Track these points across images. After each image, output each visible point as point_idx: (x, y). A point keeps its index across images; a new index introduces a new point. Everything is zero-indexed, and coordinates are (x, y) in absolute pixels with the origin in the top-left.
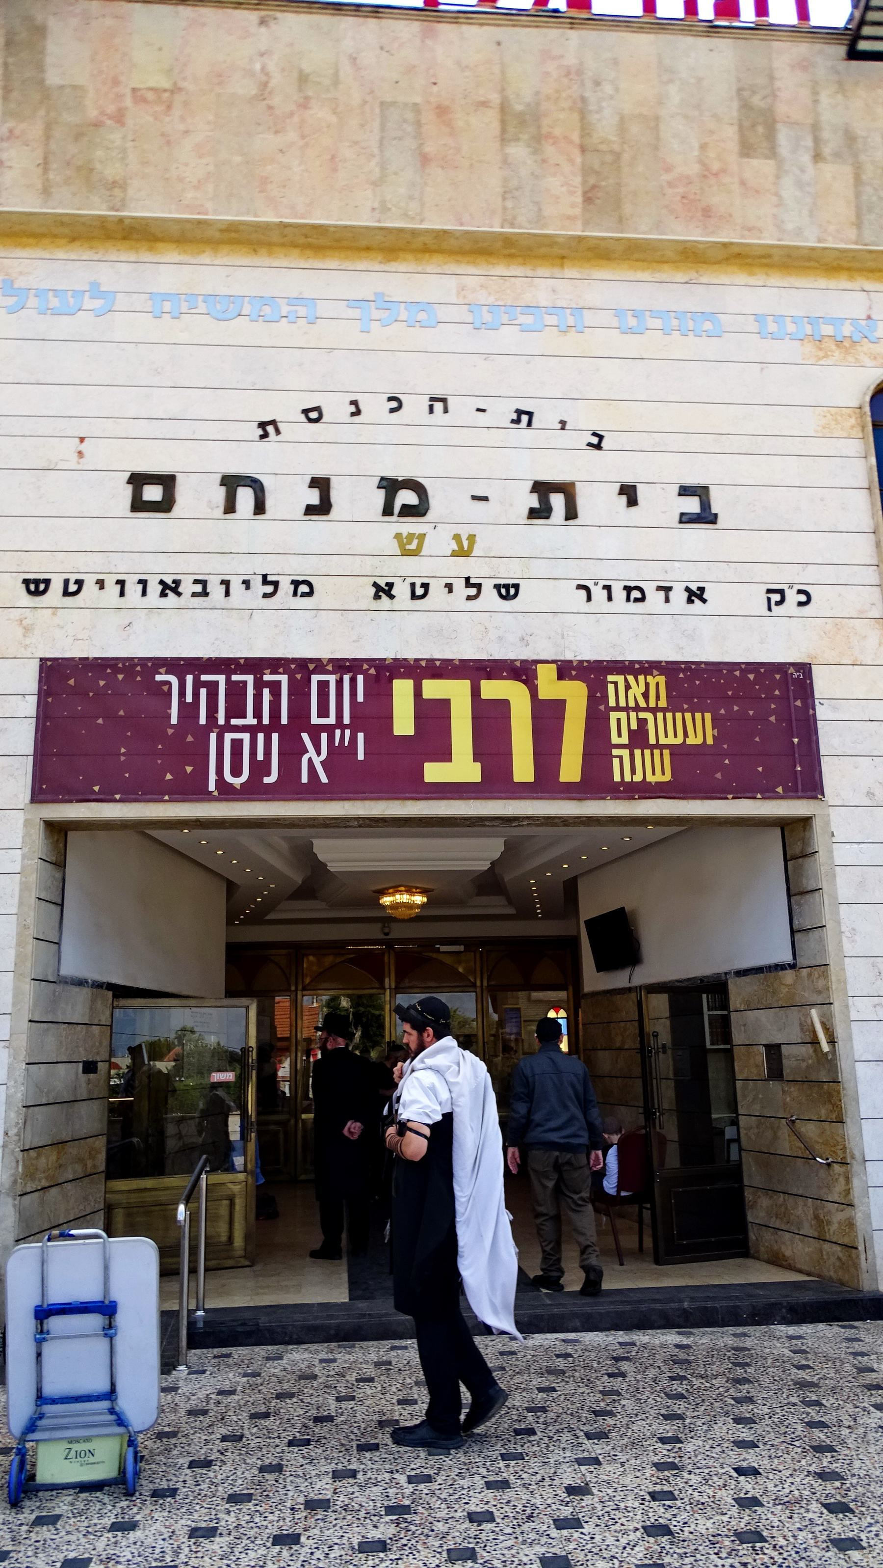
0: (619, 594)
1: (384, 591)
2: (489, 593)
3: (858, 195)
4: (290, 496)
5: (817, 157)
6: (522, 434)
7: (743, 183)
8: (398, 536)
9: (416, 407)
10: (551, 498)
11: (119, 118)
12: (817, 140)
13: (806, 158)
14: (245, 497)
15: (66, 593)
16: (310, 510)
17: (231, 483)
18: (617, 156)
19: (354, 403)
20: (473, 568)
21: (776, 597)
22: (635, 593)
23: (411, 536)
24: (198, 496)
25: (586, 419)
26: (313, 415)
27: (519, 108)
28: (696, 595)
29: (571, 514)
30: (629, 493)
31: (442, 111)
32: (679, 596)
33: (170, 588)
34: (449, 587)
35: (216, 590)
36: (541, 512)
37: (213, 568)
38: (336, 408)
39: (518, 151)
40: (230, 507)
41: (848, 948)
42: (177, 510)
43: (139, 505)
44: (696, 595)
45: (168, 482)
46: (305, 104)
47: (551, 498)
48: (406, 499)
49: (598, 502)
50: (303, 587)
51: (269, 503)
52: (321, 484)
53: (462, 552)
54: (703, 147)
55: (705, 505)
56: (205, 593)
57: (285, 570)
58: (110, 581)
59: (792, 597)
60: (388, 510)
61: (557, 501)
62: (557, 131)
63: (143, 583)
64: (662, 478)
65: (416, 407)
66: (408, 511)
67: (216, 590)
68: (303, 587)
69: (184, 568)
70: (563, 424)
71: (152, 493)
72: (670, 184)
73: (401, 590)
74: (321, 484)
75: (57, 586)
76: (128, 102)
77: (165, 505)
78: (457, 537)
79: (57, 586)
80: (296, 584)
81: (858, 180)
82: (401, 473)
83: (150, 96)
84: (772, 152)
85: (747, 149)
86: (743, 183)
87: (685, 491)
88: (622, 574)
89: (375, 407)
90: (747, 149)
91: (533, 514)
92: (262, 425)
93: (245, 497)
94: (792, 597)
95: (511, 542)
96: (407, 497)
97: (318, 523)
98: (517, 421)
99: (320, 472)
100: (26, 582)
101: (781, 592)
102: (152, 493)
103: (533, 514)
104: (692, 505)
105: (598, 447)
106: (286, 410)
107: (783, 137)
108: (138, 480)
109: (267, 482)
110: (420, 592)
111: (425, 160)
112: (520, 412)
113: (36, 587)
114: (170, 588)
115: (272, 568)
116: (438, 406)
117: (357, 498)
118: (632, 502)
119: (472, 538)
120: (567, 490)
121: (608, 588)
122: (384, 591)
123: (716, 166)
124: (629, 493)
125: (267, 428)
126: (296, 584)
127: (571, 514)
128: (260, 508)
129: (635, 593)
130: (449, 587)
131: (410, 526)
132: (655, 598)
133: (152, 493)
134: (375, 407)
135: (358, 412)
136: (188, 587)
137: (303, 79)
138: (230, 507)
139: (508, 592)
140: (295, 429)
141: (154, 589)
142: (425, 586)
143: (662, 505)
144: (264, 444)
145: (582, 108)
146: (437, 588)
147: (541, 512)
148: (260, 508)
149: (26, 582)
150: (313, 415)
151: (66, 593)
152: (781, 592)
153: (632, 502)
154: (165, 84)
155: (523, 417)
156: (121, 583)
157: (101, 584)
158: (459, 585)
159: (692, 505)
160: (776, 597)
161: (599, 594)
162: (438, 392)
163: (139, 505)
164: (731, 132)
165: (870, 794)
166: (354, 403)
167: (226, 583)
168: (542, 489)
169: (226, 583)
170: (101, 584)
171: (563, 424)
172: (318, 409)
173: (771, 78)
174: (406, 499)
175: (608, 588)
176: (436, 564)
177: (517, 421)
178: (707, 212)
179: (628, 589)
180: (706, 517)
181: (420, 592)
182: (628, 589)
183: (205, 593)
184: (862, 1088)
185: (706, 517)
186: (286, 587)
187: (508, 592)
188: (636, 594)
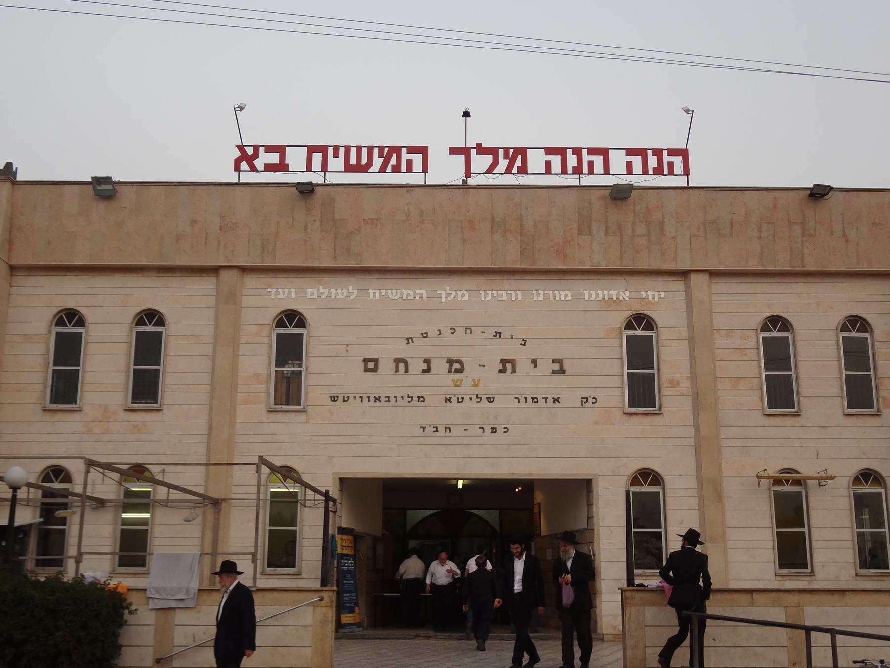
0: (529, 400)
1: (449, 400)
2: (484, 400)
3: (621, 247)
4: (417, 366)
5: (607, 233)
6: (498, 341)
7: (579, 245)
8: (453, 380)
9: (460, 331)
10: (507, 365)
11: (359, 230)
12: (606, 227)
13: (602, 234)
14: (402, 366)
15: (344, 401)
16: (424, 371)
17: (397, 361)
18: (533, 236)
19: (439, 330)
20: (480, 392)
21: (585, 400)
22: (535, 400)
23: (458, 380)
24: (386, 366)
25: (520, 334)
26: (425, 335)
27: (498, 220)
28: (556, 400)
29: (514, 371)
30: (534, 363)
31: (471, 222)
32: (550, 401)
33: (378, 399)
34: (471, 398)
35: (392, 400)
36: (503, 371)
37: (391, 392)
38: (433, 332)
39: (497, 236)
40: (397, 370)
41: (601, 524)
42: (379, 371)
43: (367, 370)
44: (556, 400)
45: (376, 361)
46: (422, 222)
47: (507, 365)
48: (456, 366)
49: (524, 366)
50: (421, 399)
51: (410, 368)
52: (427, 361)
53: (475, 386)
54: (565, 231)
55: (561, 366)
56: (389, 401)
57: (416, 392)
58: (358, 397)
59: (591, 400)
60: (450, 371)
61: (509, 366)
62: (512, 228)
63: (369, 397)
64: (545, 355)
65: (460, 331)
66: (458, 371)
67: (392, 400)
68: (421, 399)
69: (382, 392)
70: (512, 336)
71: (371, 365)
72: (552, 247)
73: (454, 400)
74: (427, 361)
75: (341, 399)
76: (362, 224)
77: (375, 370)
78: (474, 380)
79: (341, 399)
80: (419, 397)
81: (621, 242)
82: (454, 357)
83: (370, 221)
84: (590, 233)
85: (580, 232)
86: (579, 245)
87: (554, 361)
88: (530, 393)
89: (446, 332)
90: (580, 232)
91: (501, 371)
92: (407, 339)
93: (402, 366)
94: (591, 400)
95: (492, 381)
96: (457, 366)
97: (426, 375)
98: (496, 336)
99: (427, 357)
100: (331, 397)
101: (587, 399)
102: (371, 365)
103: (501, 371)
104: (557, 367)
105: (524, 345)
106: (416, 334)
107: (594, 227)
108: (366, 361)
109: (409, 360)
110: (461, 400)
111: (464, 240)
112: (497, 332)
113: (334, 399)
114: (378, 399)
115: (410, 391)
116: (468, 331)
117: (440, 367)
118: (535, 366)
119: (479, 380)
120: (512, 362)
121: (525, 398)
122: (449, 400)
123: (569, 239)
124: (534, 363)
125: (409, 340)
126: (419, 397)
127: (514, 371)
128: (407, 371)
129: (535, 400)
130: (471, 398)
131: (457, 376)
132: (542, 401)
133: (371, 365)
134: (446, 332)
135: (440, 334)
136: (383, 399)
137: (422, 213)
138: (397, 370)
139: (491, 400)
140: (419, 340)
141: (372, 399)
142: (462, 398)
143: (546, 366)
144: (408, 347)
145: (520, 219)
146: (466, 399)
147: (503, 371)
148: (407, 371)
149: (331, 397)
150: (425, 335)
151: (344, 401)
152: (587, 399)
153: (535, 366)
154: (375, 217)
155: (498, 334)
156: (361, 397)
157: (355, 397)
158: (474, 397)
159: (557, 367)
160: (585, 400)
161: (522, 400)
162: (468, 325)
163: (367, 370)
164: (575, 225)
165: (613, 471)
166: (439, 330)
167: (396, 397)
168: (504, 362)
169: (396, 397)
170: (355, 397)
171: (512, 336)
172: (426, 333)
173: (590, 203)
174: (456, 366)
175: (525, 398)
176: (466, 390)
177: (496, 336)
178: (565, 256)
179: (533, 398)
180: (562, 371)
181: (461, 400)
182: (533, 398)
183: (389, 401)
184: (602, 570)
185: (562, 371)
186: (415, 399)
187: (491, 400)
188: (535, 400)
